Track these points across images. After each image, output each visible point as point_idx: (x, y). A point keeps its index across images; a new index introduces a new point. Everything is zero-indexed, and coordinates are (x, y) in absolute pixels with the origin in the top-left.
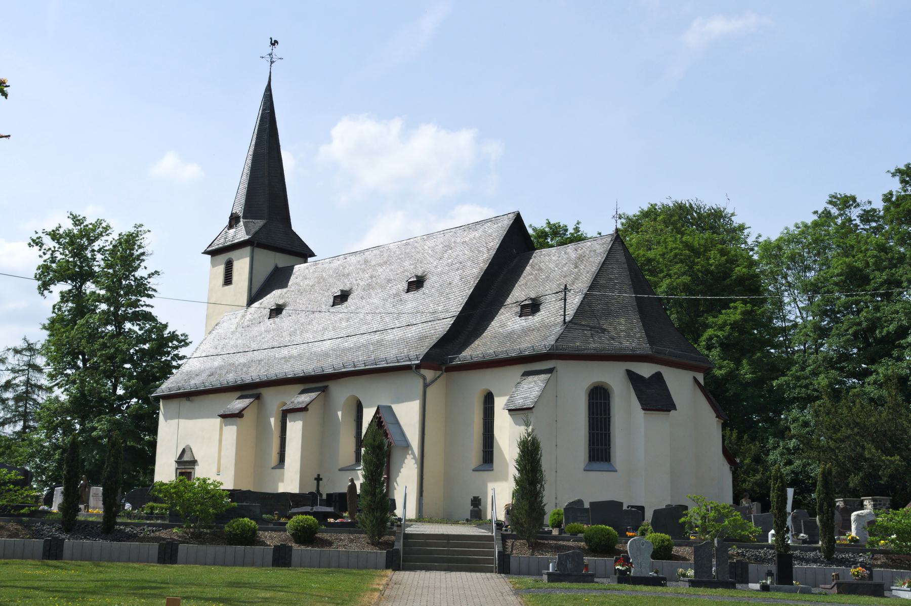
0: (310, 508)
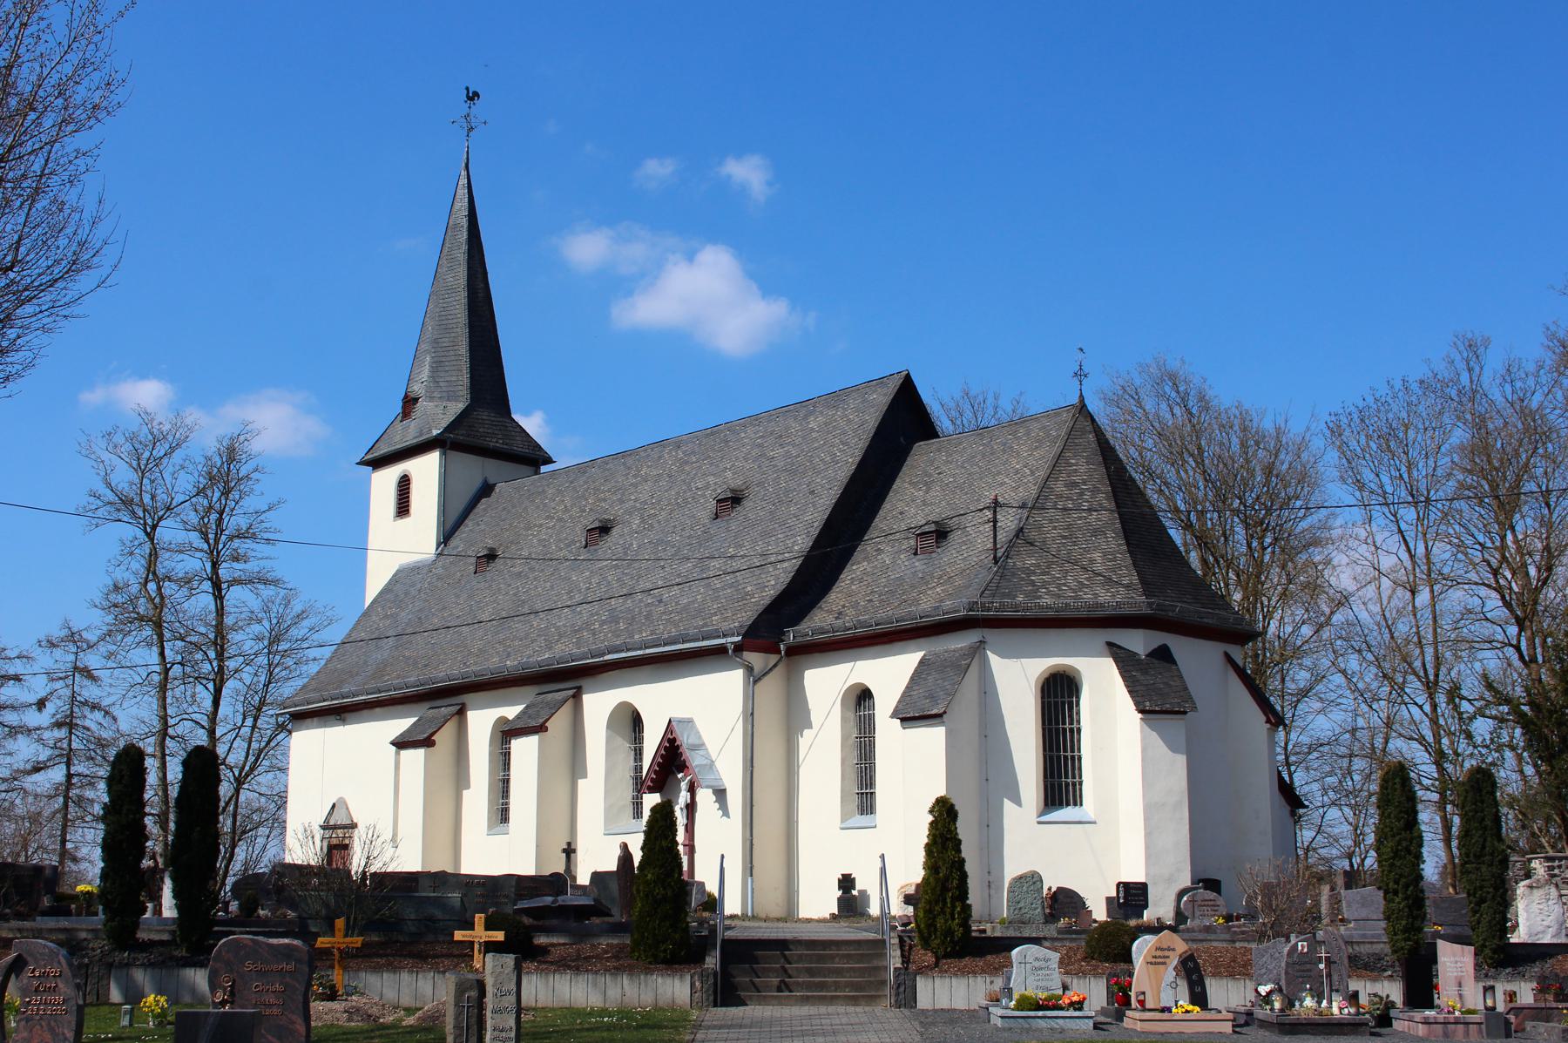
0: (550, 899)
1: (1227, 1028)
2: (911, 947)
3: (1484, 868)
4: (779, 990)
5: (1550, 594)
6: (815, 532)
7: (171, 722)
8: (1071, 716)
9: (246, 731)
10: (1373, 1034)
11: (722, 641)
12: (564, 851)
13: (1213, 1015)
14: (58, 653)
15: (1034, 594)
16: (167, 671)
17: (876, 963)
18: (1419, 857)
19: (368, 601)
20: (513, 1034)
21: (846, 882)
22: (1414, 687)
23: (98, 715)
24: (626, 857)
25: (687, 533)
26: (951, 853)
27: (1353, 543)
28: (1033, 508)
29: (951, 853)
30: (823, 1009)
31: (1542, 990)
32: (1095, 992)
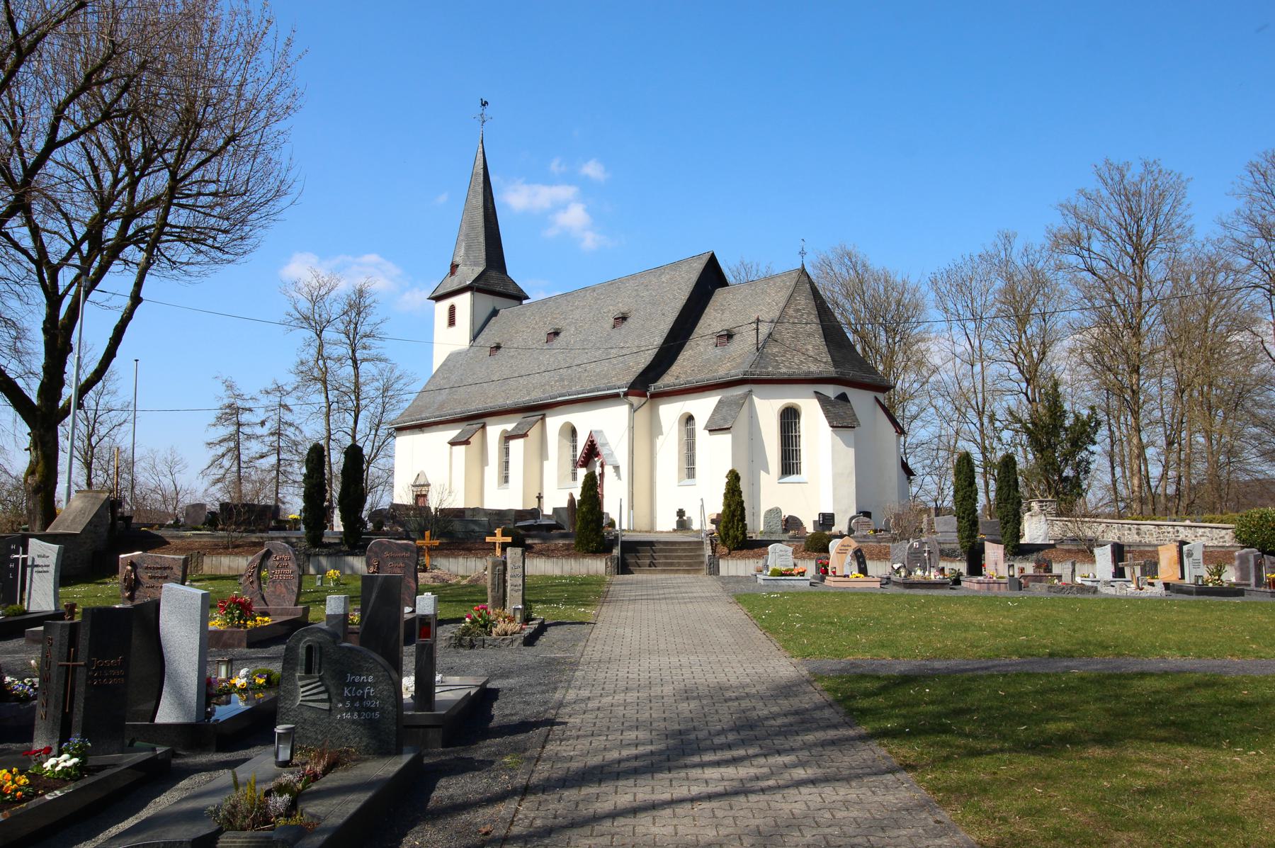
1: (878, 585)
2: (716, 545)
3: (1009, 506)
4: (650, 566)
5: (1043, 366)
6: (665, 335)
7: (332, 432)
8: (795, 429)
9: (371, 437)
10: (951, 589)
11: (618, 391)
12: (537, 497)
13: (870, 579)
14: (271, 397)
15: (777, 367)
16: (330, 406)
17: (698, 553)
18: (975, 500)
19: (434, 370)
20: (521, 588)
21: (681, 513)
22: (972, 415)
23: (292, 429)
24: (572, 501)
25: (598, 336)
26: (737, 498)
27: (941, 340)
28: (777, 322)
29: (737, 498)
30: (672, 576)
31: (1038, 566)
32: (810, 567)
